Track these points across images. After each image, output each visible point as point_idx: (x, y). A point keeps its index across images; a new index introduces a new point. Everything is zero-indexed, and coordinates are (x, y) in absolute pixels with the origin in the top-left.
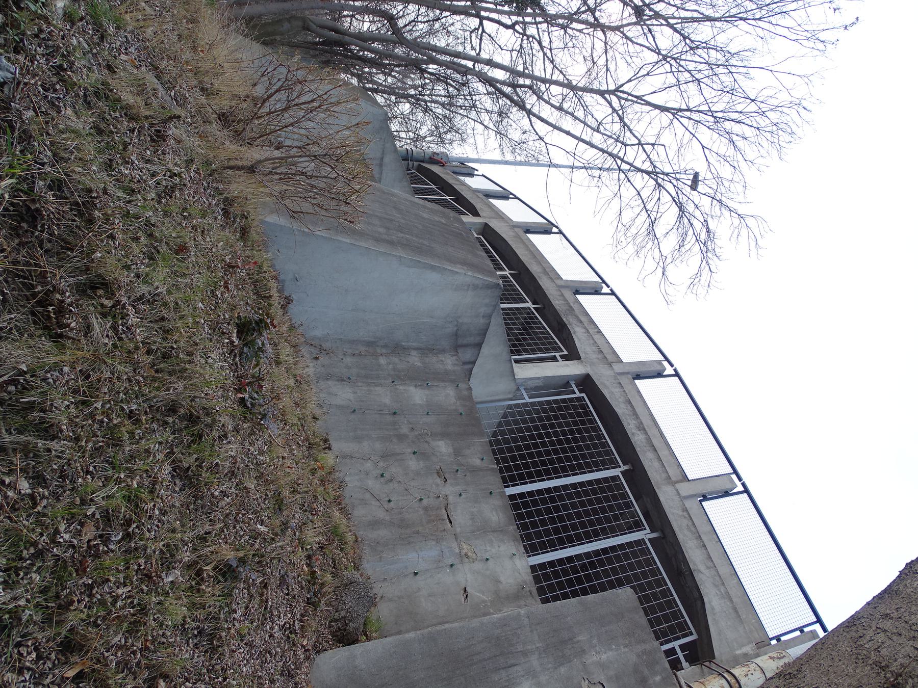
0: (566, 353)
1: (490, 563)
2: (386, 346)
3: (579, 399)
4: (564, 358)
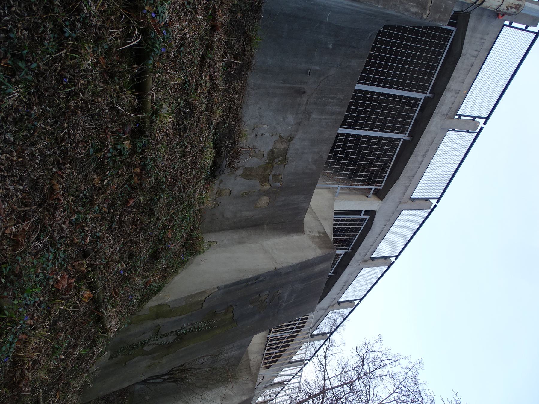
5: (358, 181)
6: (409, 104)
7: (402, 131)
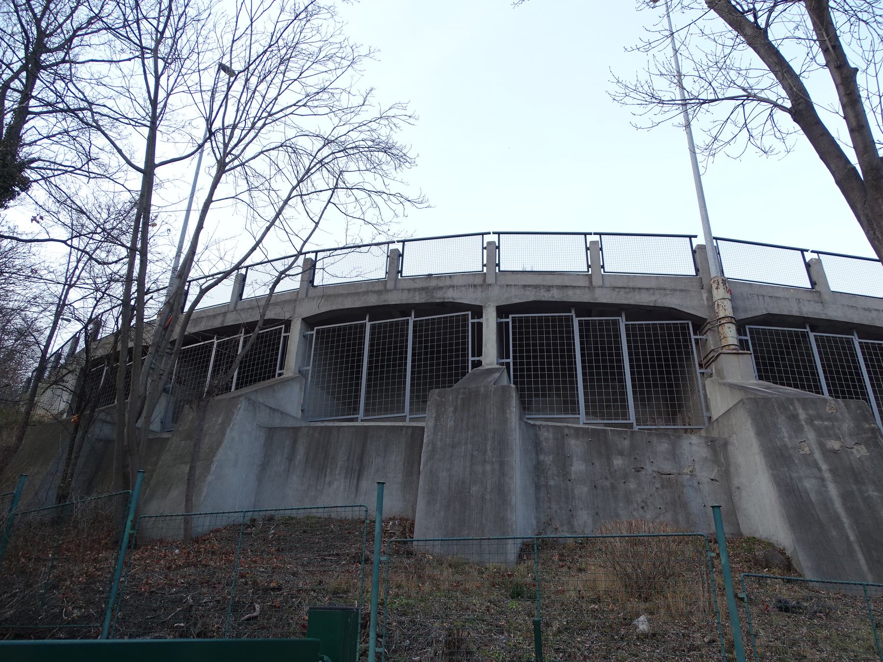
0: (283, 326)
1: (696, 459)
2: (538, 477)
3: (318, 331)
4: (287, 330)
5: (687, 353)
6: (587, 330)
7: (850, 342)
